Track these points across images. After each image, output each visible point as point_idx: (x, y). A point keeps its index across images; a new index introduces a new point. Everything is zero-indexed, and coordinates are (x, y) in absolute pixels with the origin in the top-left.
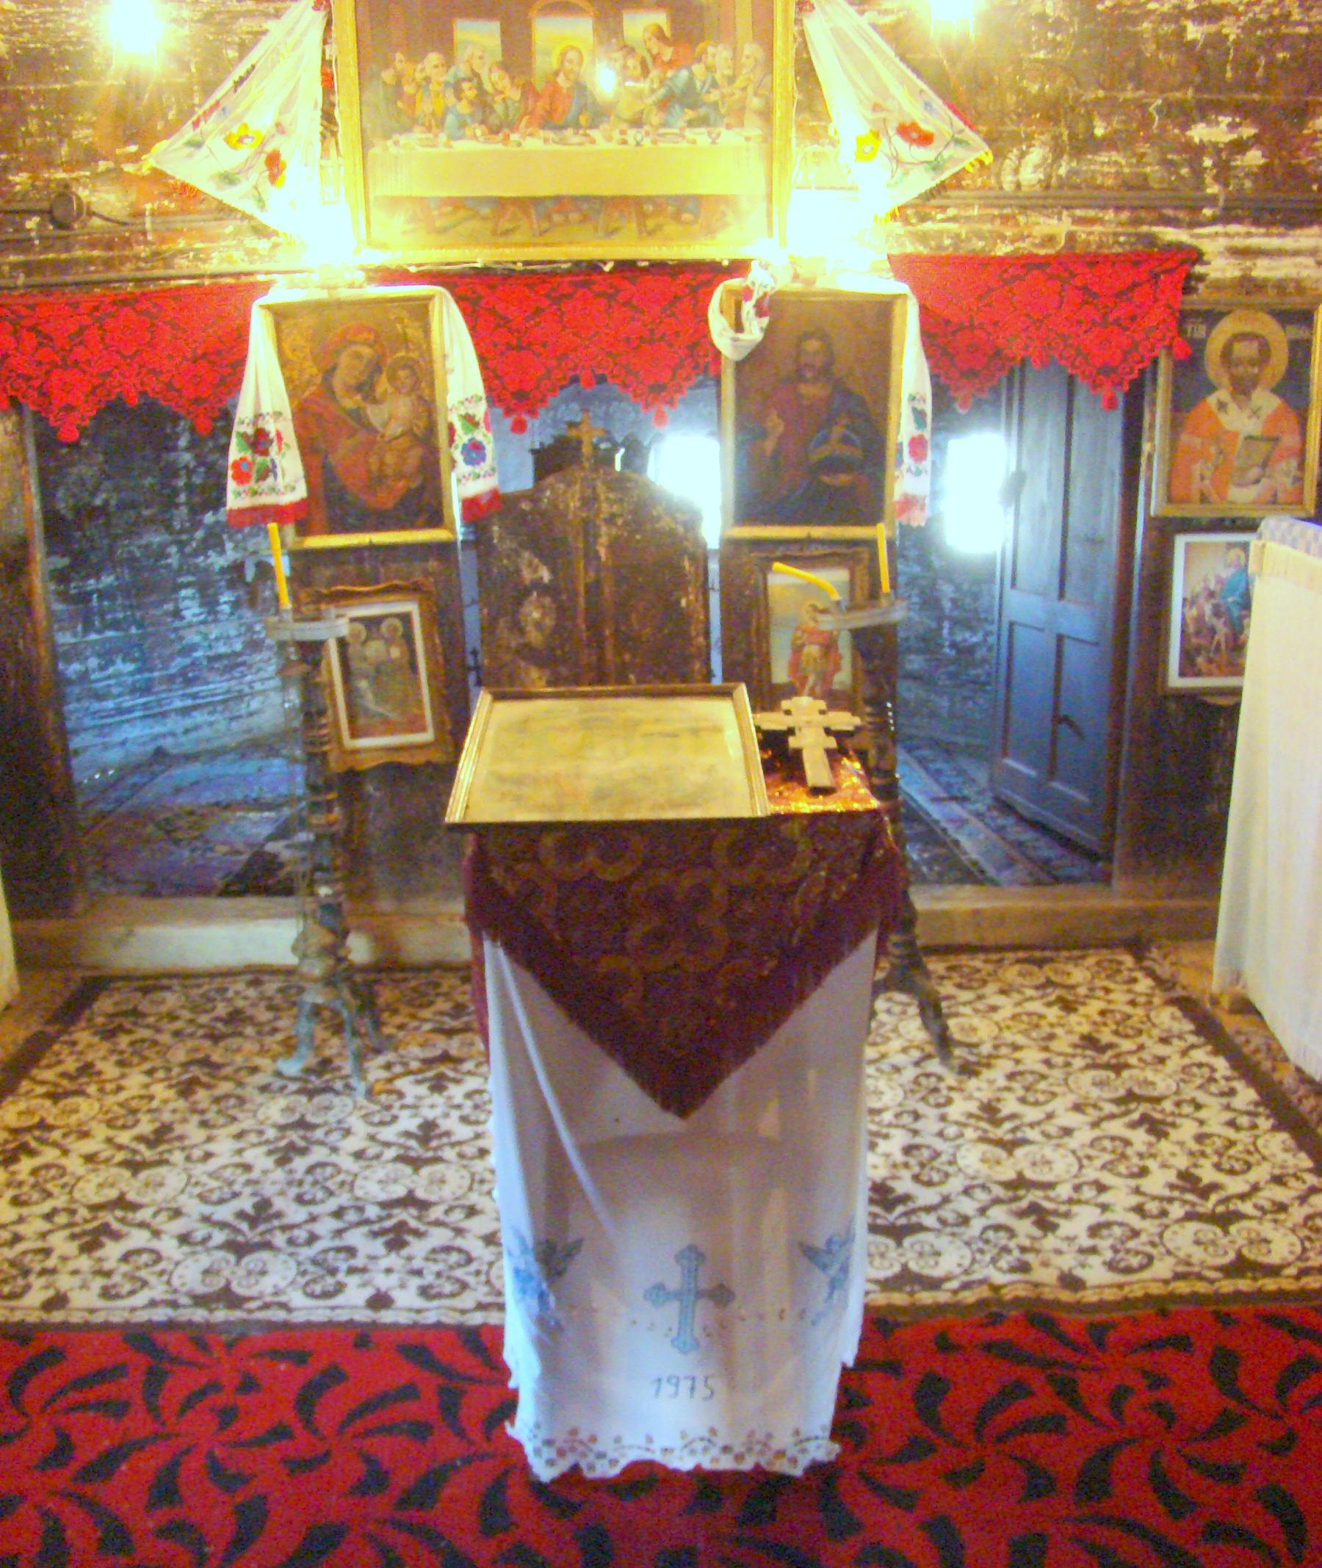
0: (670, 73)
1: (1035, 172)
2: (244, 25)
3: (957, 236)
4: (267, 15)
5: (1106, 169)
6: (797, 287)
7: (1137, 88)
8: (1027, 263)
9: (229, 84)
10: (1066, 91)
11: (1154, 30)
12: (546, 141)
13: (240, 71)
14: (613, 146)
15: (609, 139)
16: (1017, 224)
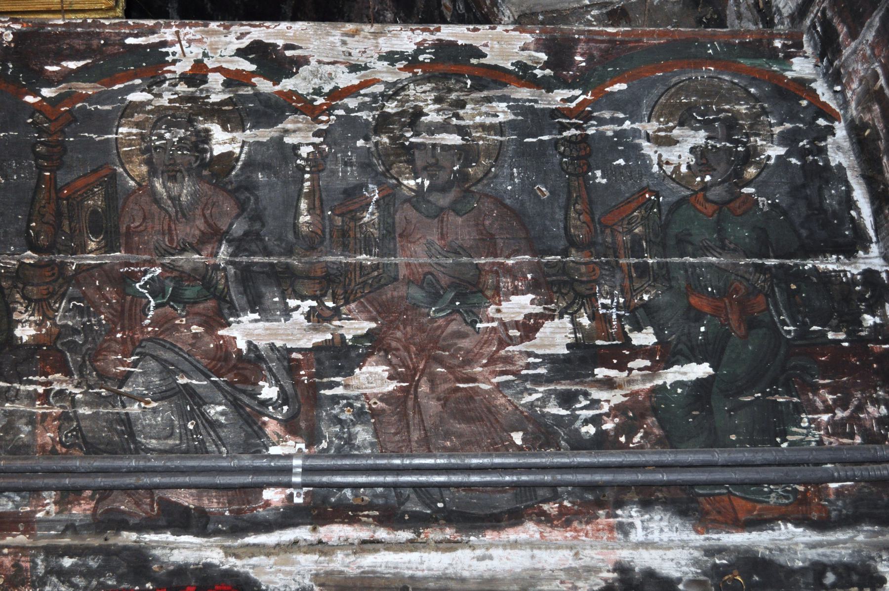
5: (39, 409)
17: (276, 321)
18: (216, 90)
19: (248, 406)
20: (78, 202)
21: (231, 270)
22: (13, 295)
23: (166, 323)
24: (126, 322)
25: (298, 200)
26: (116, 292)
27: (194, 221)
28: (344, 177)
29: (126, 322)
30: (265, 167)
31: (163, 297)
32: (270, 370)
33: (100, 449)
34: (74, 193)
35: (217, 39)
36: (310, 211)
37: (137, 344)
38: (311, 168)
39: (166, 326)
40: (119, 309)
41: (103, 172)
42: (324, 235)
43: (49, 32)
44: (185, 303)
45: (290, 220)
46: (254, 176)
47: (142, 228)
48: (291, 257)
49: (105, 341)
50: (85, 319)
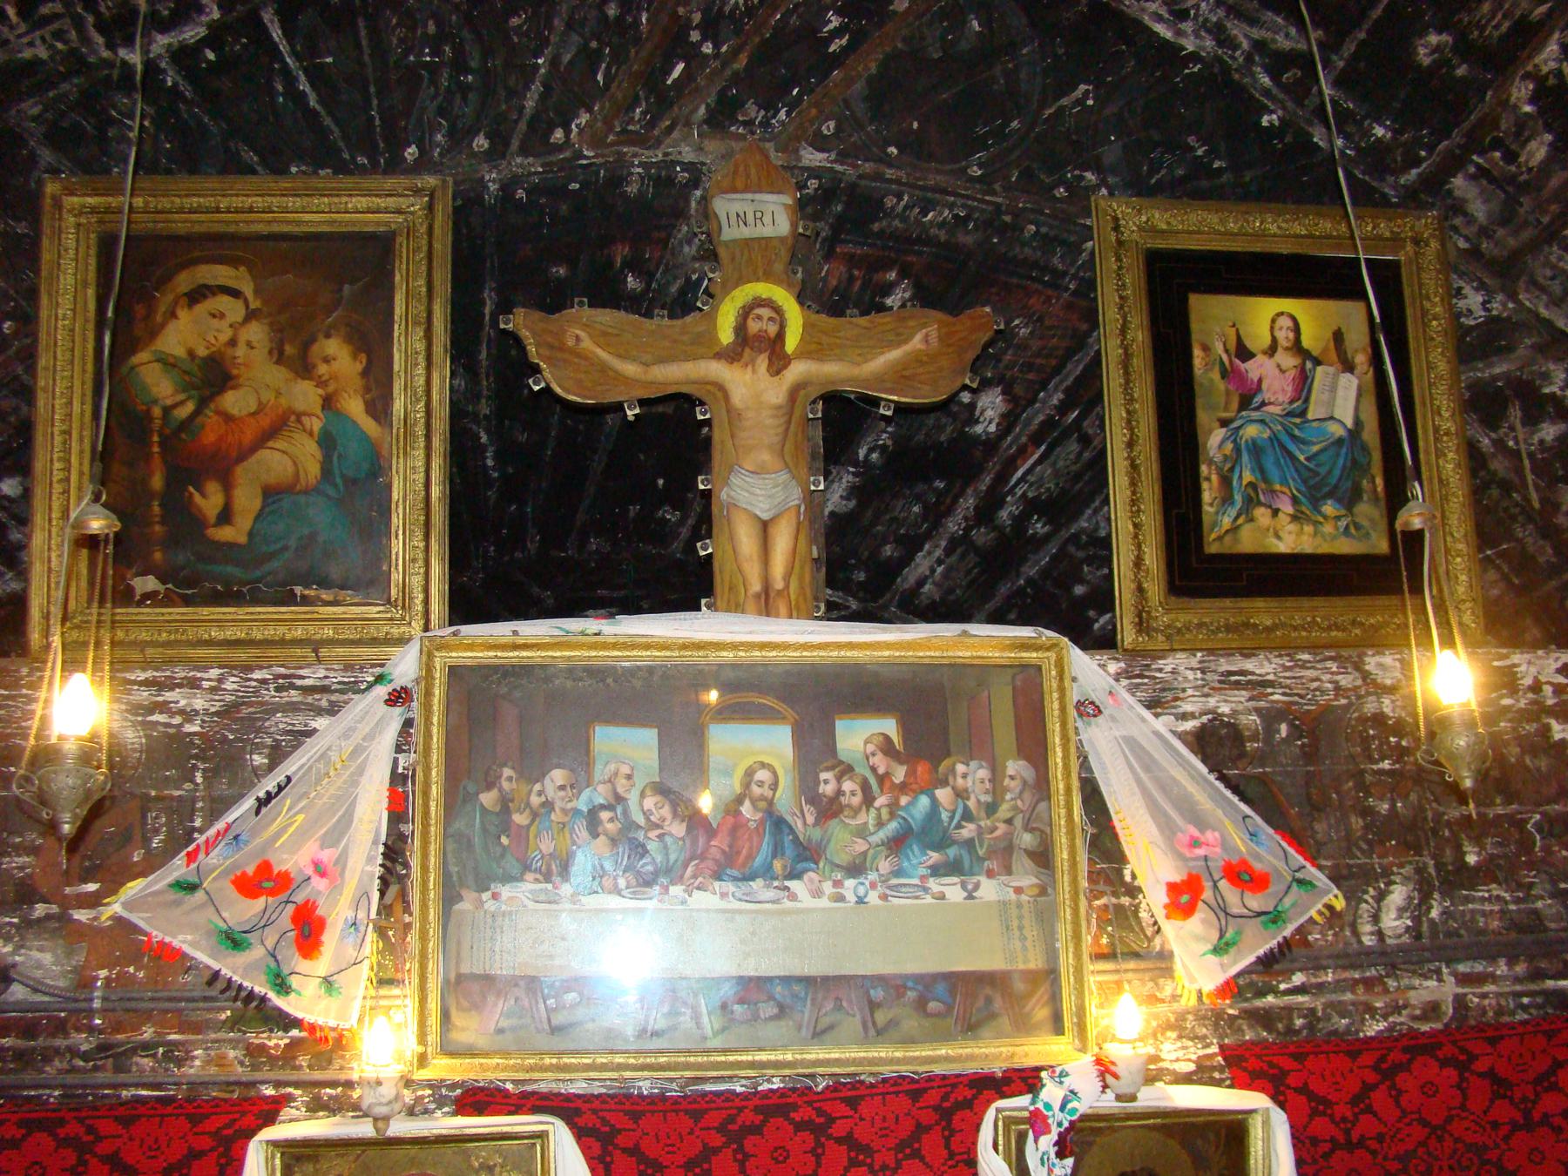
0: (904, 800)
1: (1399, 917)
2: (281, 721)
3: (1312, 1011)
4: (320, 712)
5: (1487, 907)
6: (1108, 1103)
7: (1507, 802)
8: (1406, 1048)
9: (249, 803)
10: (1423, 810)
11: (1514, 729)
12: (724, 895)
13: (270, 784)
14: (824, 902)
15: (817, 893)
16: (1386, 991)
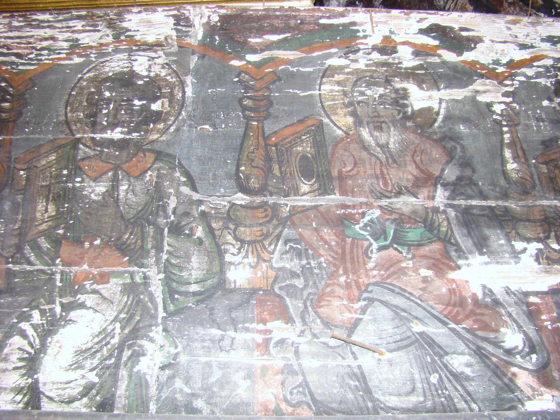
1: (77, 366)
17: (506, 263)
18: (406, 58)
19: (493, 355)
20: (287, 149)
21: (452, 213)
22: (225, 237)
23: (391, 266)
24: (349, 265)
25: (502, 150)
26: (335, 234)
27: (406, 165)
28: (539, 131)
29: (349, 265)
30: (465, 120)
31: (386, 239)
32: (510, 315)
33: (333, 409)
34: (282, 140)
35: (399, 22)
36: (516, 158)
37: (363, 288)
38: (507, 122)
39: (392, 269)
40: (340, 251)
41: (309, 122)
42: (534, 180)
43: (251, 15)
44: (409, 246)
45: (498, 166)
46: (456, 128)
47: (354, 172)
48: (507, 201)
49: (328, 285)
50: (304, 262)
